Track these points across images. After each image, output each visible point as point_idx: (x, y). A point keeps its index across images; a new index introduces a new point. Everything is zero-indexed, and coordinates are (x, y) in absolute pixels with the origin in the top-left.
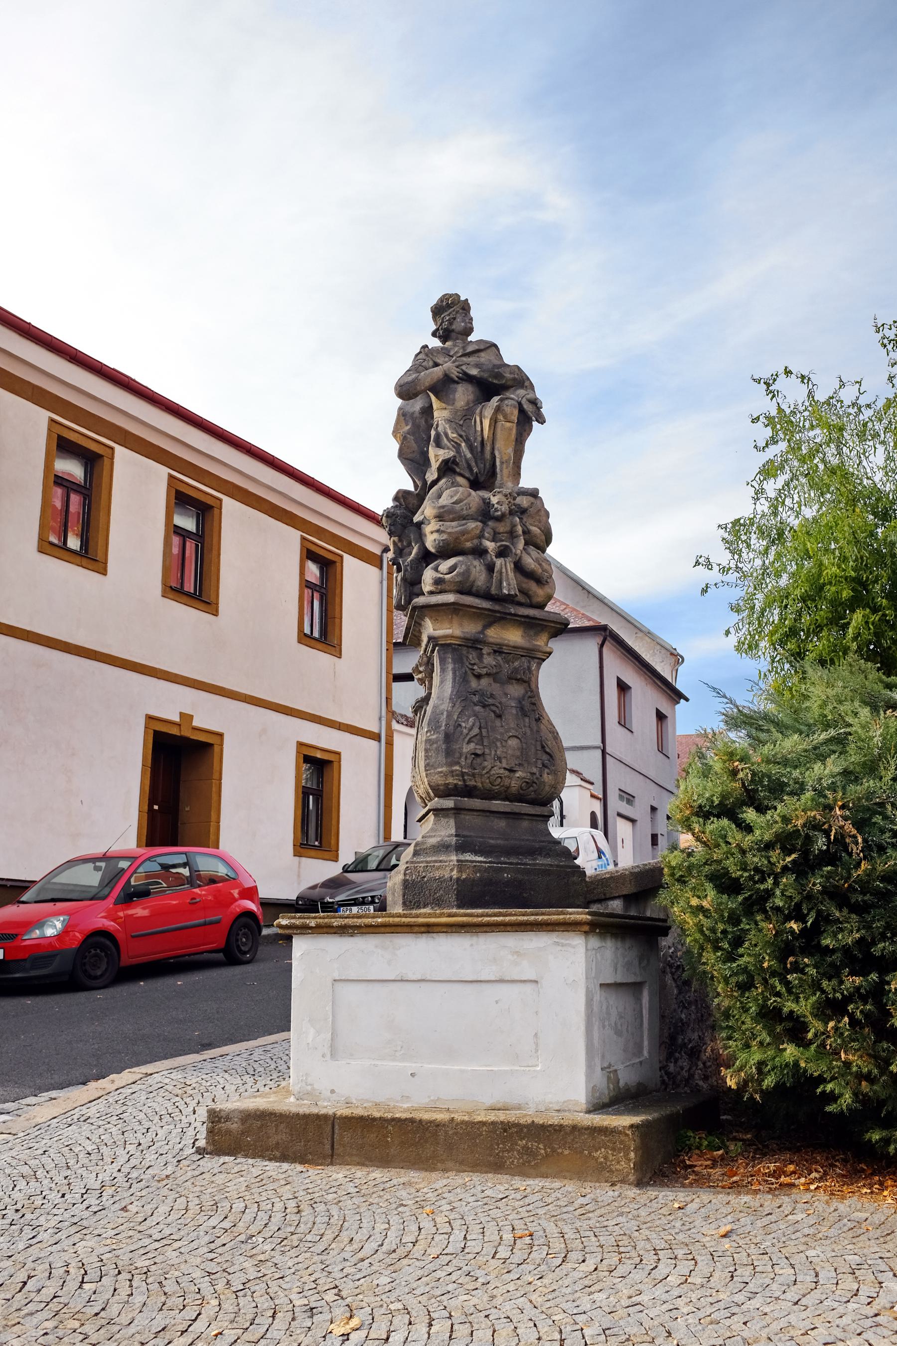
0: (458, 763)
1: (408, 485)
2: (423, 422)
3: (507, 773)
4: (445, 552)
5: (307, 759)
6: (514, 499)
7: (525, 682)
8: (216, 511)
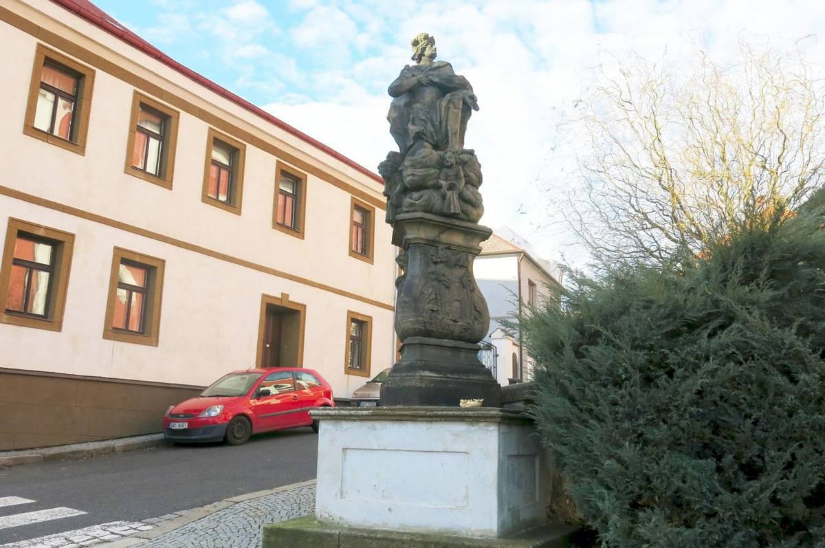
0: (421, 316)
1: (396, 149)
2: (405, 111)
3: (452, 323)
4: (419, 187)
5: (353, 320)
6: (459, 155)
7: (464, 267)
8: (304, 182)
